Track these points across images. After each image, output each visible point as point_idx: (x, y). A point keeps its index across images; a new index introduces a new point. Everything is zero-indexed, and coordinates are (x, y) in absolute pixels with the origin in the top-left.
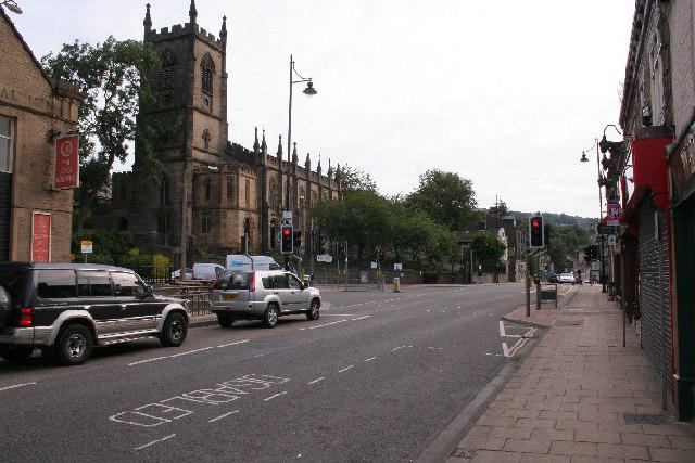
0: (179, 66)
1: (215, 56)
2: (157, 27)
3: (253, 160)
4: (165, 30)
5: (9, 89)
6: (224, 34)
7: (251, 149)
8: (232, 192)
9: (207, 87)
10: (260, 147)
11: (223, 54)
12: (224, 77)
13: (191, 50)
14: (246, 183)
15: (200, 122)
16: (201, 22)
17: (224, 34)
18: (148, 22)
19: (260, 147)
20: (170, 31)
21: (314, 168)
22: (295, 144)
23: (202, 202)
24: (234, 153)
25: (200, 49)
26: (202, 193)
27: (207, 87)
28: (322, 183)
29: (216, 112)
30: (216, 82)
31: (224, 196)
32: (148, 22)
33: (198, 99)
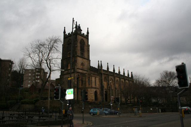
0: (76, 43)
1: (85, 39)
2: (67, 33)
3: (99, 71)
4: (69, 34)
5: (171, 66)
6: (88, 33)
7: (97, 68)
8: (90, 82)
9: (82, 49)
10: (100, 67)
11: (88, 39)
12: (88, 46)
13: (76, 38)
14: (95, 81)
15: (80, 60)
16: (110, 70)
17: (88, 33)
18: (65, 32)
19: (100, 67)
20: (70, 33)
21: (126, 75)
22: (101, 62)
23: (80, 86)
24: (93, 69)
25: (79, 38)
26: (80, 83)
27: (82, 49)
28: (125, 78)
29: (86, 56)
30: (86, 48)
31: (87, 84)
32: (65, 32)
33: (79, 53)
